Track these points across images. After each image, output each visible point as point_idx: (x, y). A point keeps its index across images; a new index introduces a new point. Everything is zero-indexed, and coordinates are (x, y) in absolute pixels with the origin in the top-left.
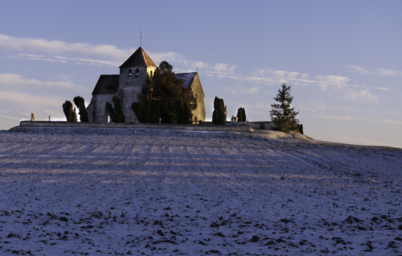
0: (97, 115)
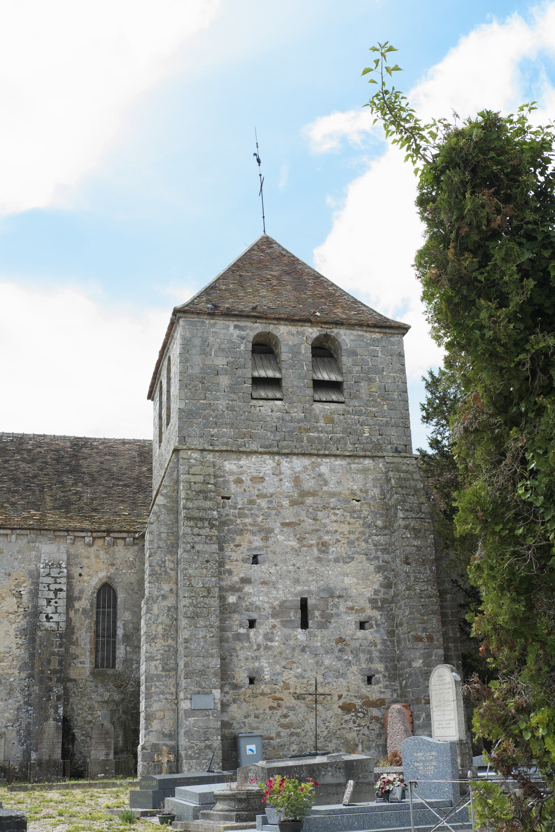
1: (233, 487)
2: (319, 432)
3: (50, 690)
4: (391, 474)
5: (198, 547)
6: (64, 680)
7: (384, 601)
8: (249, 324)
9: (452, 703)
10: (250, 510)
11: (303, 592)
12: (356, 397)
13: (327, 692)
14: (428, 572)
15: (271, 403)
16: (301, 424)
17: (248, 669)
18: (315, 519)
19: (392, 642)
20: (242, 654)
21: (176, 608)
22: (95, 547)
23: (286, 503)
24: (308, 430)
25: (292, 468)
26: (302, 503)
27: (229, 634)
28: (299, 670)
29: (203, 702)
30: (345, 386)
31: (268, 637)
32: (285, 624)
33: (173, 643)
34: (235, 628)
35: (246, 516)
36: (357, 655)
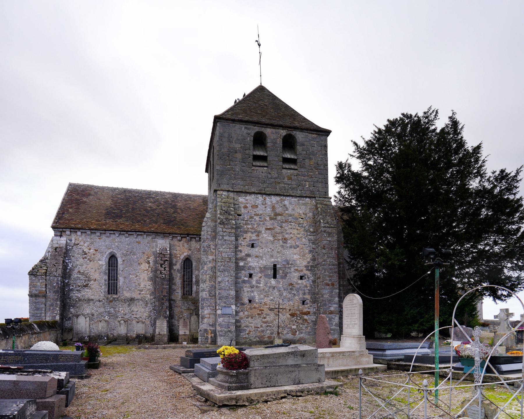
0: (75, 295)
1: (242, 209)
2: (285, 184)
3: (163, 304)
4: (318, 206)
5: (225, 238)
6: (170, 300)
7: (312, 266)
8: (252, 127)
9: (357, 315)
10: (251, 221)
11: (275, 261)
12: (303, 167)
13: (284, 307)
14: (334, 253)
15: (262, 168)
16: (276, 180)
17: (248, 296)
18: (281, 227)
19: (315, 286)
20: (245, 289)
21: (215, 267)
22: (182, 242)
23: (268, 218)
24: (279, 183)
25: (271, 202)
26: (276, 219)
27: (240, 280)
28: (272, 298)
29: (227, 311)
30: (298, 161)
31: (258, 282)
32: (266, 276)
33: (214, 284)
34: (243, 277)
35: (249, 224)
36: (298, 291)
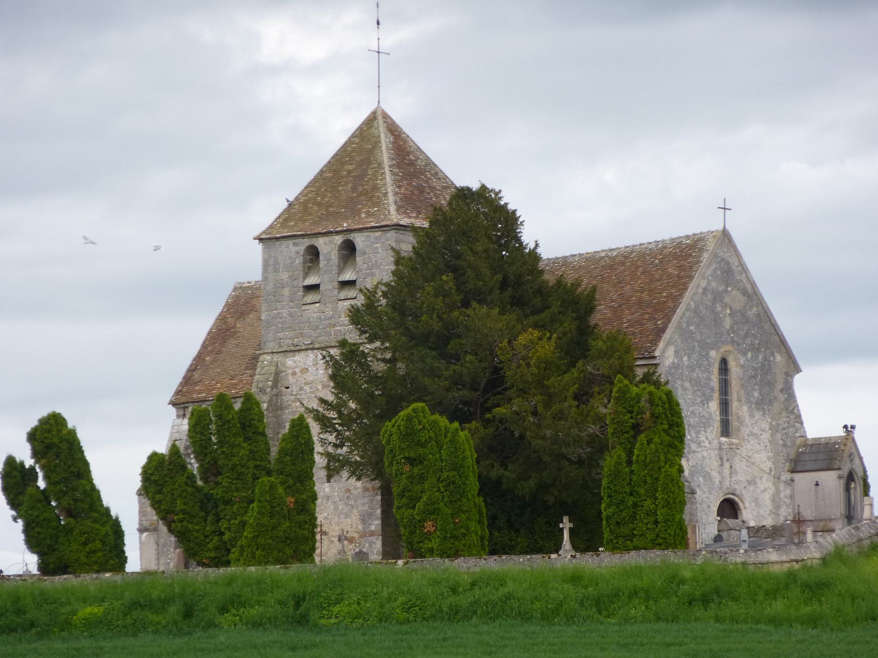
1: (290, 377)
15: (313, 306)
23: (320, 387)
